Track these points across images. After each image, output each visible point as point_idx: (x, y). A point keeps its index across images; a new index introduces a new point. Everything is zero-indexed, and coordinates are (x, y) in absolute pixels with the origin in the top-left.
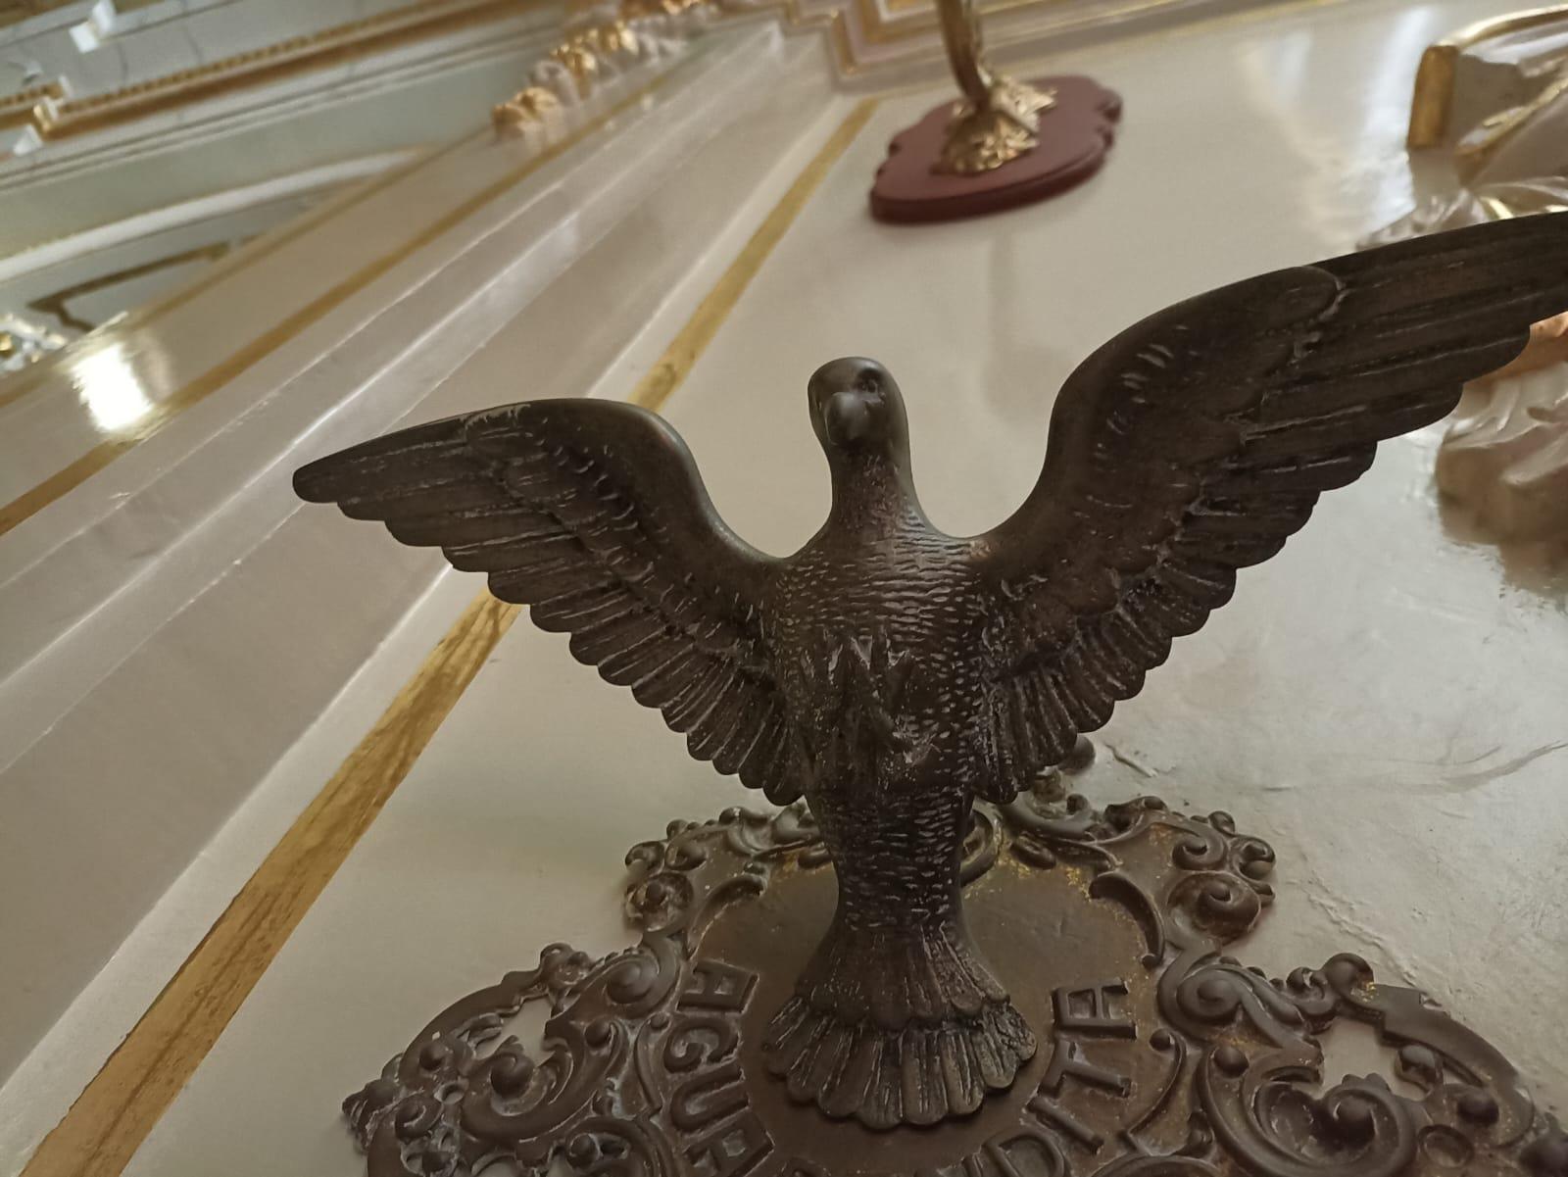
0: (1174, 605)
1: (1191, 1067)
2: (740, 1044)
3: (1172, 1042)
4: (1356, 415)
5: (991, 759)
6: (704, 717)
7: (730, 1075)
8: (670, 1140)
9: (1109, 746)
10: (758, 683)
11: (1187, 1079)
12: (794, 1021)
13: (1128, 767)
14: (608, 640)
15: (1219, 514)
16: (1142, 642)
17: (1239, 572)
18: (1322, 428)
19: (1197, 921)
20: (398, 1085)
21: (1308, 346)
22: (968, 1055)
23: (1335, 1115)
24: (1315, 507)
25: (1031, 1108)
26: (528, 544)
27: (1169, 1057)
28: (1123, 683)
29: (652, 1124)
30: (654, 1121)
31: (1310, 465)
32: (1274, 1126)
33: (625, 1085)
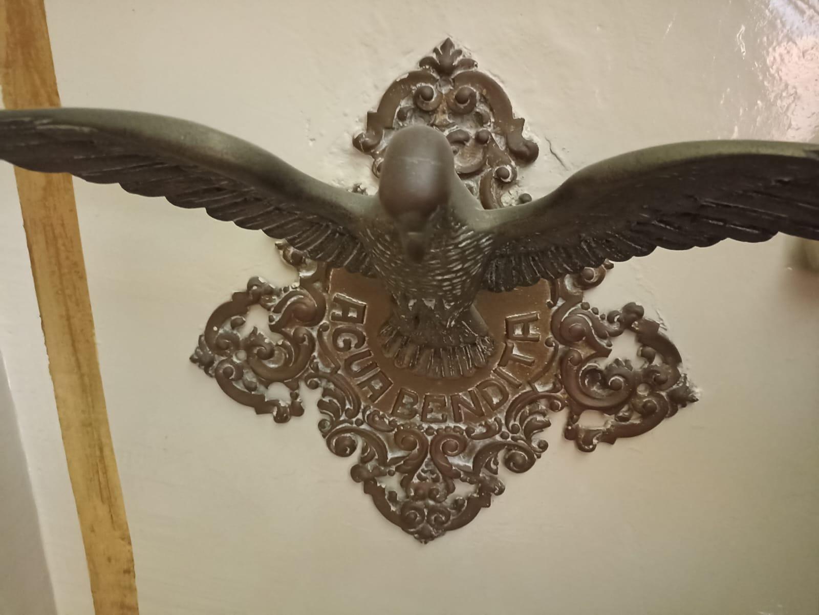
0: (613, 250)
1: (560, 354)
2: (367, 339)
3: (554, 345)
4: (779, 217)
5: (492, 281)
6: (316, 244)
7: (367, 353)
8: (349, 380)
9: (548, 141)
10: (361, 271)
11: (557, 358)
12: (390, 335)
13: (558, 161)
14: (234, 211)
15: (662, 225)
16: (589, 258)
17: (658, 248)
18: (754, 214)
19: (576, 283)
20: (212, 355)
21: (780, 181)
22: (470, 354)
23: (609, 384)
24: (721, 241)
25: (495, 371)
26: (140, 169)
27: (552, 349)
28: (571, 269)
29: (339, 374)
30: (339, 372)
31: (732, 226)
32: (586, 382)
33: (320, 355)
